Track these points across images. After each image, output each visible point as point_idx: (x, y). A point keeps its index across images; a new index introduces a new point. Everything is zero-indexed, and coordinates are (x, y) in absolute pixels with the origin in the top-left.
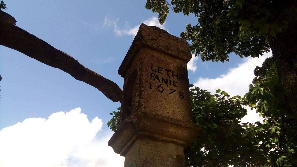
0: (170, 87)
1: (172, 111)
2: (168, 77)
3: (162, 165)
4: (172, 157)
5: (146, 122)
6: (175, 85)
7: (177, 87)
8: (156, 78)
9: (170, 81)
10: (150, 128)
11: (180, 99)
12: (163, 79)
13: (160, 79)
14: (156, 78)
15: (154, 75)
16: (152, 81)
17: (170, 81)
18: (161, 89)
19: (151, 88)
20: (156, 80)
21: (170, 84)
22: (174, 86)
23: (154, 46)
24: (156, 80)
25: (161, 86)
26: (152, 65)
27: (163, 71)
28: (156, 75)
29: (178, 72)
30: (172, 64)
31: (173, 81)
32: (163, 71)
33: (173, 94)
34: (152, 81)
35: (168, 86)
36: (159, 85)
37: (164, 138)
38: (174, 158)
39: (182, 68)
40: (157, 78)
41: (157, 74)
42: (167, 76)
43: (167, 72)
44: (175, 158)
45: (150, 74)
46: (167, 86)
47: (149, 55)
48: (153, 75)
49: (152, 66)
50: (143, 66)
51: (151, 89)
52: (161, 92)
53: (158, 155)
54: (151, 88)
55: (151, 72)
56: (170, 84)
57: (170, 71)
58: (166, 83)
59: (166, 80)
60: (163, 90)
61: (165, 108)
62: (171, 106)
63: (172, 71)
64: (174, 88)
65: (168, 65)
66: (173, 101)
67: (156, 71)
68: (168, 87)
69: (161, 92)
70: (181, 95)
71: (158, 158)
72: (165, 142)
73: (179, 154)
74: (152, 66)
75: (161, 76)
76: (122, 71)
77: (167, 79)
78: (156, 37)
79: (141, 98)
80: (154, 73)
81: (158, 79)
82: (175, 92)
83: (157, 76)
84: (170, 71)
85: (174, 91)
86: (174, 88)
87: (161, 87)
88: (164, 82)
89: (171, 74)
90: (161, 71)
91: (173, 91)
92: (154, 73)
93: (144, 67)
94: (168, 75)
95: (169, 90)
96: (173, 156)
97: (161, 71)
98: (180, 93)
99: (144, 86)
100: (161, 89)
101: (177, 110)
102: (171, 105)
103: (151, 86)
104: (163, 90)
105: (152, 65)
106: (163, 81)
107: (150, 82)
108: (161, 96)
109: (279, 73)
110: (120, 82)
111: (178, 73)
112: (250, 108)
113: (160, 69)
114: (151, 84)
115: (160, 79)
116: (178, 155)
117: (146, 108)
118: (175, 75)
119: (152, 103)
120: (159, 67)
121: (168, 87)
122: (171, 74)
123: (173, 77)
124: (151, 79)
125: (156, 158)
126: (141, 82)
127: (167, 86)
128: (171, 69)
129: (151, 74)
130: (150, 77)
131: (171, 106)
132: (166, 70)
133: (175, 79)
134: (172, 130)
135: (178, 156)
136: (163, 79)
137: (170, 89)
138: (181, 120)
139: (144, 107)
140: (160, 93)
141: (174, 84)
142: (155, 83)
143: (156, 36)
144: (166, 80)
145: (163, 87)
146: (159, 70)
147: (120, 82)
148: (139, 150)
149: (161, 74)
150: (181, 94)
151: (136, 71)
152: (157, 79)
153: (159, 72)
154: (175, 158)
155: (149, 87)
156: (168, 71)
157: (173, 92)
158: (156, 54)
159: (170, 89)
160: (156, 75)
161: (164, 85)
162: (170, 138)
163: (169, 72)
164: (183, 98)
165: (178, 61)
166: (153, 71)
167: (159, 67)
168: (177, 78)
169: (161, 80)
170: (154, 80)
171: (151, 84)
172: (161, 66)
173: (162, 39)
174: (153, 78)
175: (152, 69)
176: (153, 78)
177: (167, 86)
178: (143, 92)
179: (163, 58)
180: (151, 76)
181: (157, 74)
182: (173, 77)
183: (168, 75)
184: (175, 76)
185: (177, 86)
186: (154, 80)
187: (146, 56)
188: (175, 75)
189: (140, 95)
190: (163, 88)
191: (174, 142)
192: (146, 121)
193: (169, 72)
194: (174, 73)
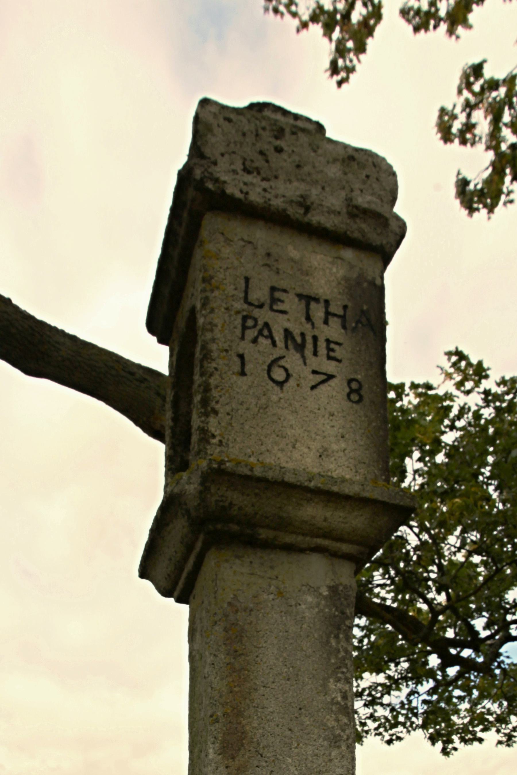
0: (314, 362)
1: (318, 451)
2: (309, 326)
3: (283, 613)
4: (315, 591)
5: (227, 490)
6: (332, 354)
7: (339, 361)
8: (260, 333)
9: (315, 339)
10: (240, 508)
11: (350, 404)
12: (288, 333)
13: (279, 337)
14: (263, 335)
15: (256, 320)
16: (246, 347)
17: (315, 339)
18: (279, 375)
19: (243, 373)
20: (261, 339)
21: (315, 354)
22: (329, 358)
23: (255, 197)
24: (261, 339)
25: (282, 362)
26: (247, 280)
27: (291, 303)
28: (260, 323)
29: (346, 302)
30: (326, 271)
31: (328, 341)
32: (291, 303)
33: (322, 387)
34: (246, 347)
35: (308, 361)
36: (272, 358)
37: (289, 539)
38: (321, 594)
39: (365, 285)
40: (266, 332)
41: (264, 315)
42: (303, 320)
43: (303, 302)
44: (326, 593)
45: (238, 321)
46: (303, 357)
47: (236, 239)
48: (250, 323)
49: (247, 287)
50: (212, 291)
51: (245, 378)
52: (281, 384)
53: (272, 587)
54: (243, 373)
55: (245, 313)
56: (315, 354)
57: (317, 300)
58: (300, 348)
59: (299, 340)
60: (288, 376)
61: (293, 440)
62: (315, 433)
63: (322, 301)
64: (330, 367)
65: (307, 275)
66: (324, 416)
67: (261, 306)
68: (305, 364)
69: (281, 384)
70: (355, 392)
71: (271, 597)
72: (290, 548)
73: (337, 582)
74: (247, 287)
75: (279, 325)
76: (161, 321)
77: (303, 335)
78: (260, 157)
79: (207, 415)
80: (256, 313)
81: (271, 337)
82: (332, 383)
83: (266, 325)
84: (317, 300)
85: (330, 377)
86: (330, 367)
87: (280, 366)
88: (291, 346)
89: (318, 312)
90: (282, 301)
91: (323, 377)
92: (256, 313)
93: (216, 293)
94: (308, 318)
95: (311, 376)
96: (319, 588)
97: (282, 301)
98: (350, 382)
99: (216, 369)
100: (279, 375)
101: (335, 447)
102: (316, 430)
103: (243, 364)
104: (288, 376)
105: (247, 280)
106: (289, 342)
107: (241, 352)
108: (280, 399)
109: (202, 484)
110: (156, 357)
111: (345, 307)
112: (453, 752)
113: (277, 295)
114: (241, 357)
115: (279, 337)
116: (333, 587)
117: (227, 445)
118: (335, 315)
119: (247, 427)
120: (273, 289)
121: (305, 364)
122: (318, 312)
123: (326, 322)
124: (243, 338)
125: (265, 596)
126: (207, 356)
127: (303, 357)
128: (321, 291)
129: (245, 319)
130: (238, 332)
131: (315, 433)
132: (300, 296)
133: (334, 331)
134: (313, 512)
135: (333, 589)
136: (288, 333)
137: (314, 372)
138: (348, 477)
139: (220, 441)
140: (277, 388)
141: (330, 350)
142: (259, 353)
143: (261, 153)
144: (299, 340)
145: (288, 366)
146: (274, 300)
147: (156, 357)
148: (215, 577)
149: (281, 316)
150: (354, 385)
151: (193, 311)
152: (266, 337)
153: (275, 307)
154: (326, 593)
155: (237, 368)
156: (308, 299)
157: (323, 382)
158: (261, 235)
159: (314, 372)
160: (260, 323)
161: (292, 360)
162: (308, 539)
163: (313, 305)
164: (360, 400)
165: (348, 254)
166: (251, 308)
167: (273, 289)
168: (344, 327)
169: (280, 341)
170: (255, 341)
171: (241, 357)
172: (283, 284)
173: (285, 161)
174: (251, 334)
175: (246, 300)
176: (251, 334)
177: (301, 362)
178: (215, 393)
179: (294, 249)
180: (244, 328)
181: (264, 315)
182: (326, 322)
183: (308, 318)
184: (336, 319)
185: (339, 358)
186: (255, 341)
187: (223, 249)
188: (335, 315)
189: (205, 402)
190: (286, 370)
191: (318, 550)
192: (225, 489)
193: (313, 305)
194: (332, 309)
